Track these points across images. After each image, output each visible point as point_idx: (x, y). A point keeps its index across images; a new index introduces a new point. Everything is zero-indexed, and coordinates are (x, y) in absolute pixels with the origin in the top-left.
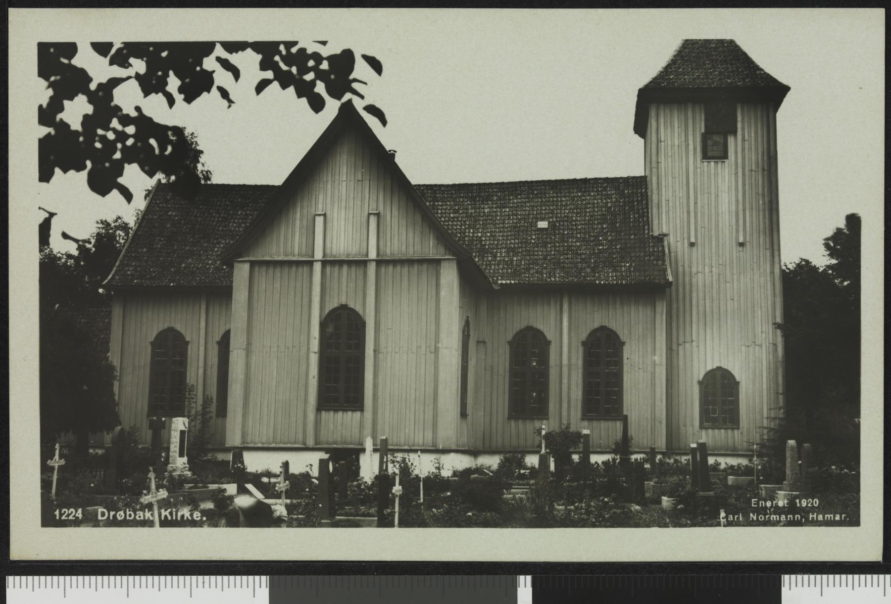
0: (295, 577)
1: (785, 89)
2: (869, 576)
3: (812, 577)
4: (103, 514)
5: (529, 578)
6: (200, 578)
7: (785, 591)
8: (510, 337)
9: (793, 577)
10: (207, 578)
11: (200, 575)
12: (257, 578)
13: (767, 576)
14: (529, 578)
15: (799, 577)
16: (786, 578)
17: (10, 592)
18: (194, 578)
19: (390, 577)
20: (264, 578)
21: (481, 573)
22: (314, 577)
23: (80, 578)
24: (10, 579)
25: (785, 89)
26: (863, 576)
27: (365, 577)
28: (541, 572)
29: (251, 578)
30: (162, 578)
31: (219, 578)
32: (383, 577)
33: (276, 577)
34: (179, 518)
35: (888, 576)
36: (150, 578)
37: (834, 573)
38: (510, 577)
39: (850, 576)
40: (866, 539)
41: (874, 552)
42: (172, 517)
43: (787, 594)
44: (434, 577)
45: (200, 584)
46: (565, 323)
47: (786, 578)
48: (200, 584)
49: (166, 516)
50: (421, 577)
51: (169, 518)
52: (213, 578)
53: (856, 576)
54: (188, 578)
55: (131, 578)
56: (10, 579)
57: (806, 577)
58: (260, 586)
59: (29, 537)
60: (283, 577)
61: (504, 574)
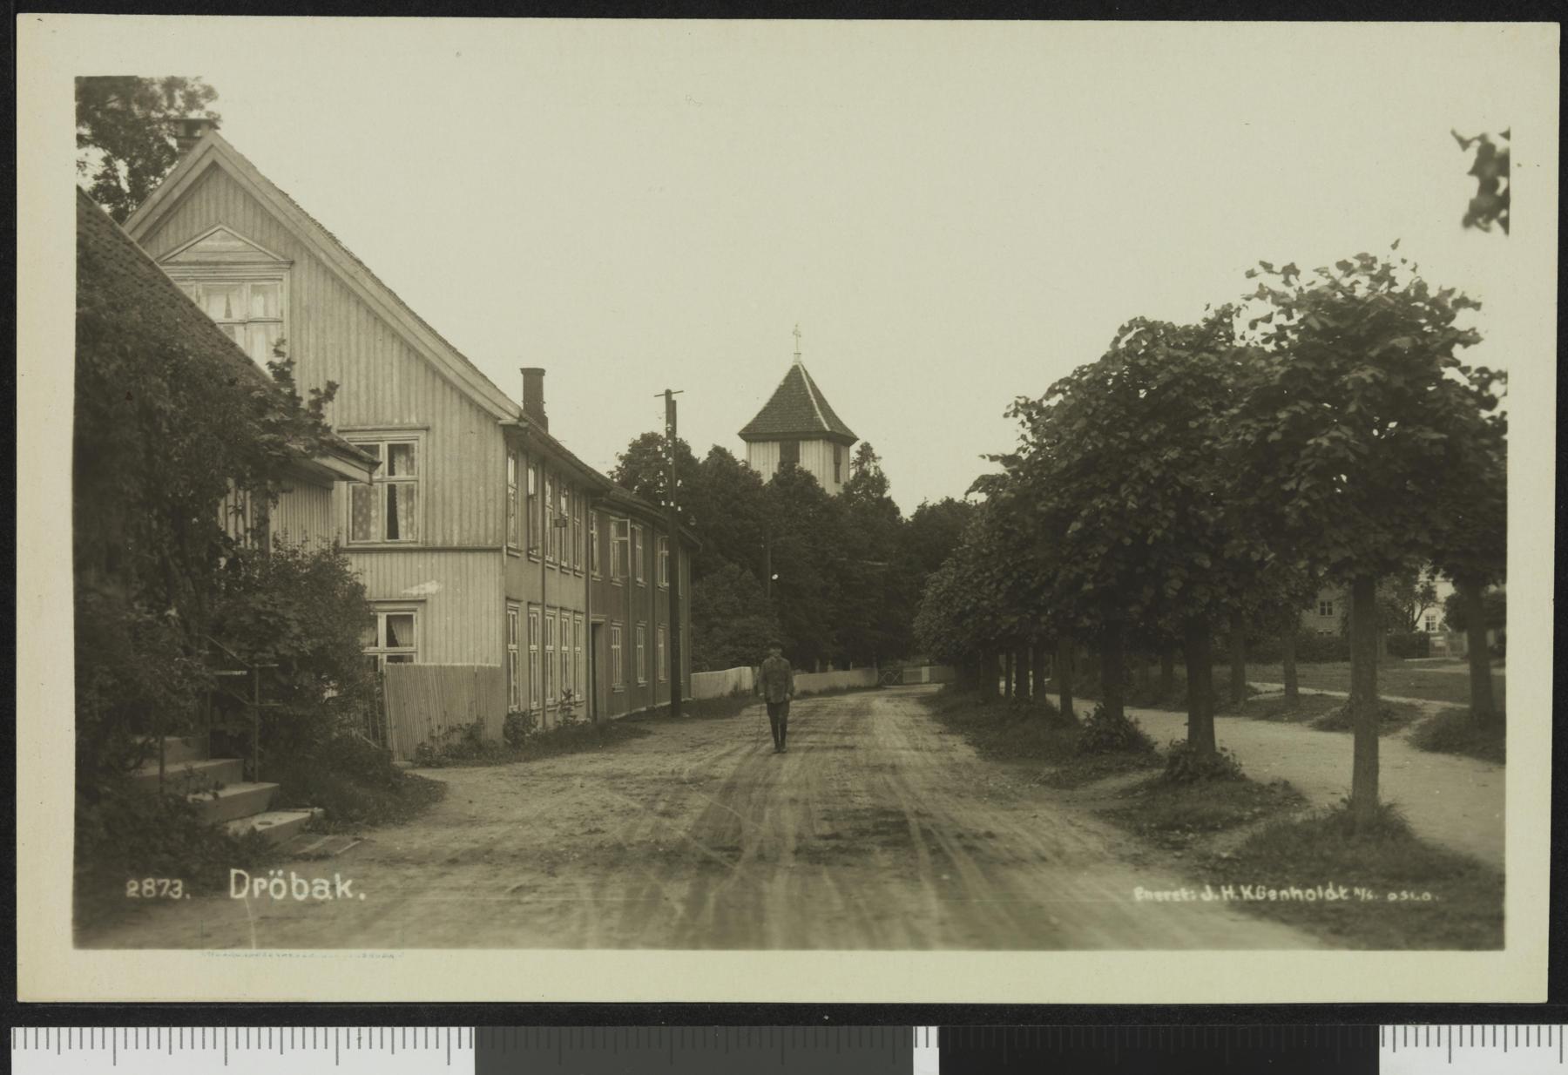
7: (1385, 1055)
9: (1400, 1028)
11: (376, 1025)
13: (1349, 1034)
16: (1387, 1031)
20: (466, 1030)
21: (756, 1023)
23: (142, 1030)
24: (18, 1033)
28: (962, 1025)
30: (398, 1030)
40: (1520, 965)
41: (1536, 991)
43: (1388, 1058)
44: (766, 1029)
45: (354, 1041)
47: (1387, 1031)
48: (354, 1041)
56: (18, 1033)
58: (460, 1045)
59: (50, 961)
60: (499, 1029)
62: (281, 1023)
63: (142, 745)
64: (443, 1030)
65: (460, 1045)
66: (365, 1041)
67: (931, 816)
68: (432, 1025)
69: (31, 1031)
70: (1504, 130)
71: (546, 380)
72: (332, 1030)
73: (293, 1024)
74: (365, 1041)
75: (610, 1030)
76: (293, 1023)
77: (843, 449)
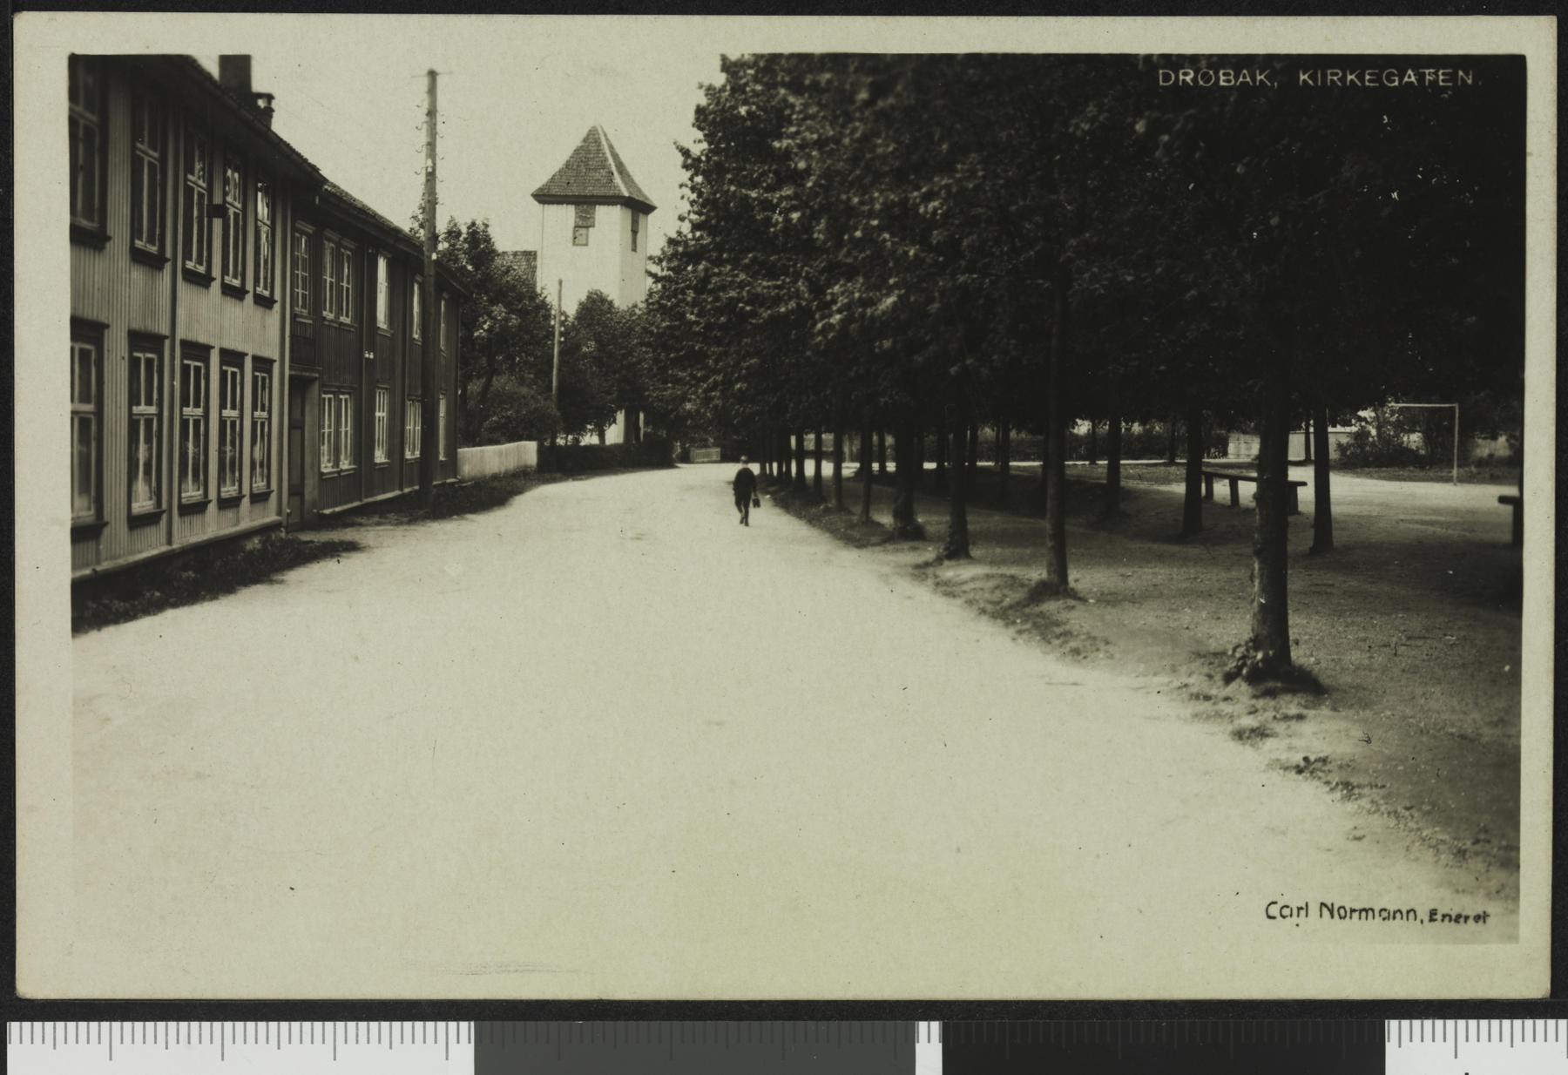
1: (74, 60)
5: (936, 1026)
7: (1391, 1048)
8: (505, 241)
9: (1405, 1023)
11: (217, 1020)
12: (452, 1025)
14: (936, 1026)
17: (13, 1050)
19: (688, 1024)
20: (464, 1025)
24: (14, 1027)
25: (74, 60)
31: (161, 1025)
35: (1563, 1023)
39: (1506, 1023)
40: (1521, 957)
41: (1537, 984)
42: (1315, 80)
45: (127, 1036)
47: (1393, 1025)
48: (127, 1036)
56: (14, 1027)
58: (460, 1040)
60: (498, 1024)
62: (111, 1018)
63: (864, 235)
64: (441, 1025)
65: (460, 1040)
66: (306, 1037)
67: (1239, 735)
68: (385, 1020)
69: (27, 1025)
70: (548, 164)
71: (80, 51)
72: (251, 1025)
74: (306, 1037)
75: (609, 1024)
76: (200, 1018)
77: (641, 217)
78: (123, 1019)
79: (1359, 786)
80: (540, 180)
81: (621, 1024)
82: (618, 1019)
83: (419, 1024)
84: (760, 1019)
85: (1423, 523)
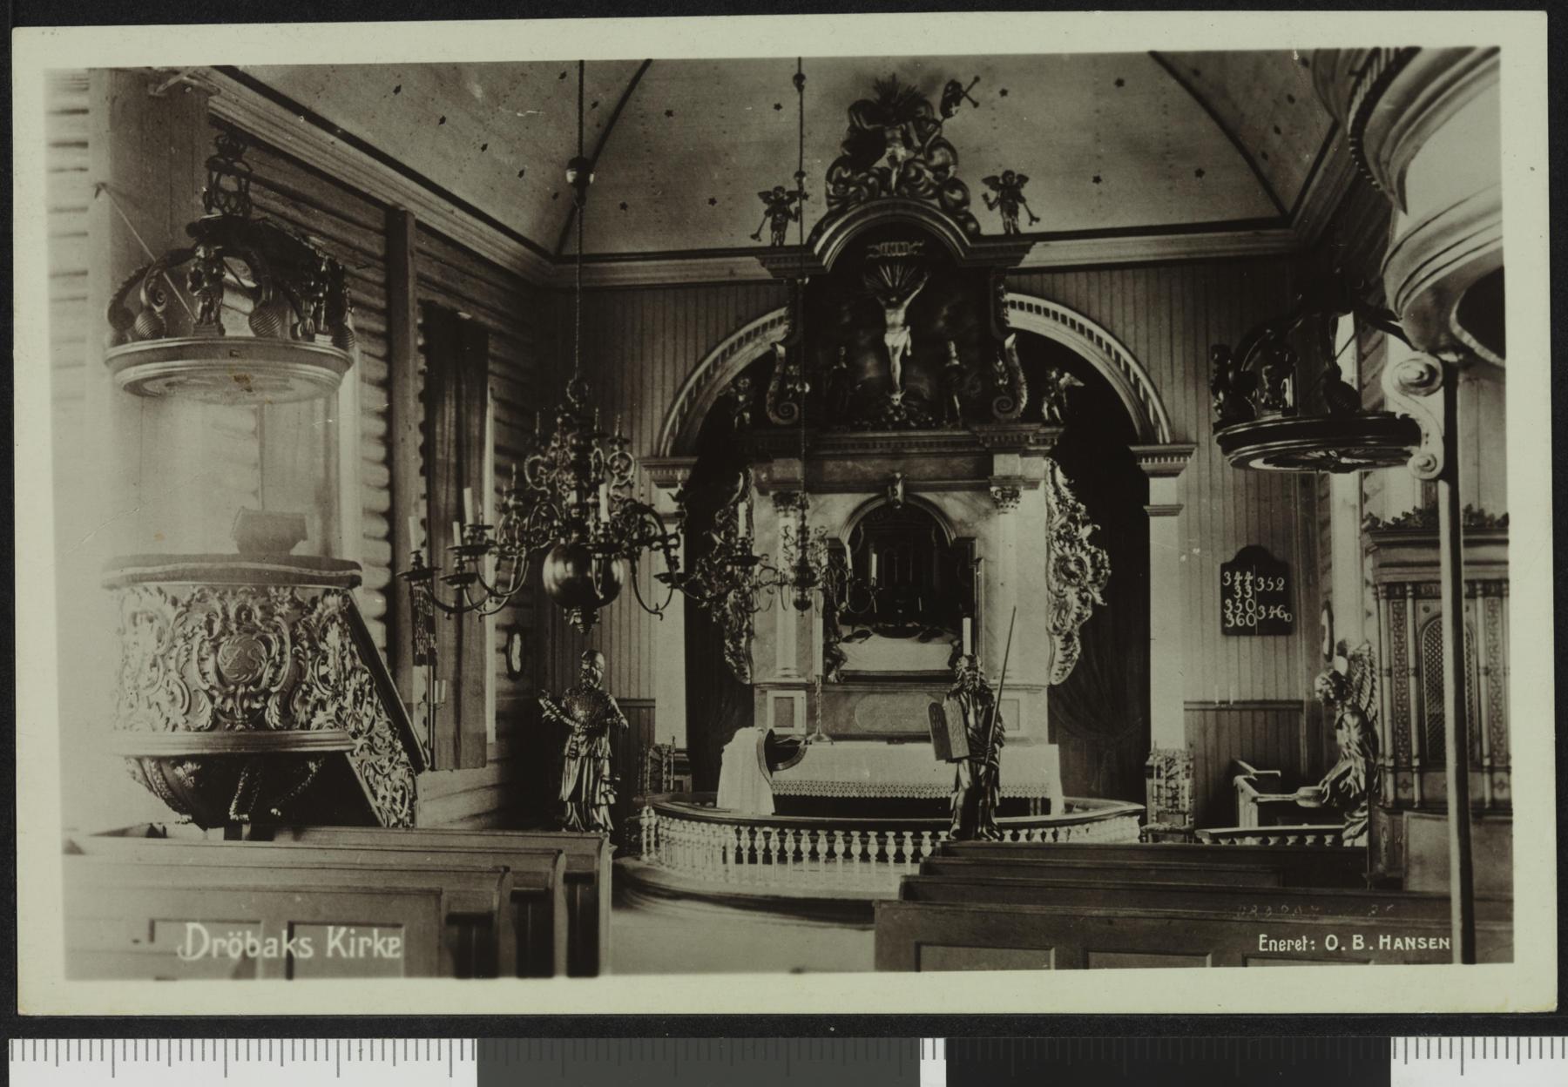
0: (524, 1041)
2: (1547, 1040)
3: (1445, 1040)
4: (1332, 943)
6: (355, 1042)
7: (1396, 1065)
9: (1412, 1040)
10: (366, 1042)
11: (175, 1037)
12: (456, 1042)
13: (1365, 1041)
15: (1423, 1040)
16: (1398, 1043)
17: (15, 1067)
18: (344, 1042)
20: (468, 1042)
22: (557, 1042)
23: (299, 1042)
24: (16, 1045)
26: (1535, 1040)
27: (647, 1041)
28: (962, 1032)
29: (445, 1042)
31: (389, 1042)
32: (681, 1041)
33: (490, 1041)
34: (361, 954)
36: (265, 1042)
37: (1462, 1033)
38: (906, 1041)
40: (1528, 975)
41: (1543, 997)
45: (355, 1054)
46: (1304, 751)
47: (1398, 1043)
48: (355, 1054)
49: (336, 950)
50: (749, 1041)
51: (344, 954)
52: (377, 1042)
53: (1524, 1040)
54: (332, 1042)
55: (231, 1042)
56: (16, 1045)
57: (1434, 1040)
60: (502, 1041)
61: (896, 1034)
62: (180, 1035)
69: (29, 1042)
73: (293, 1036)
74: (1490, 1051)
76: (293, 1035)
78: (180, 1036)
79: (261, 389)
80: (1503, 57)
81: (625, 1041)
82: (619, 1036)
83: (422, 1042)
84: (762, 1035)
85: (1470, 100)
